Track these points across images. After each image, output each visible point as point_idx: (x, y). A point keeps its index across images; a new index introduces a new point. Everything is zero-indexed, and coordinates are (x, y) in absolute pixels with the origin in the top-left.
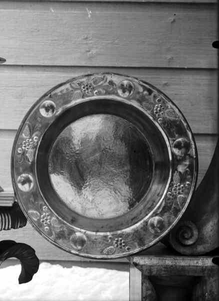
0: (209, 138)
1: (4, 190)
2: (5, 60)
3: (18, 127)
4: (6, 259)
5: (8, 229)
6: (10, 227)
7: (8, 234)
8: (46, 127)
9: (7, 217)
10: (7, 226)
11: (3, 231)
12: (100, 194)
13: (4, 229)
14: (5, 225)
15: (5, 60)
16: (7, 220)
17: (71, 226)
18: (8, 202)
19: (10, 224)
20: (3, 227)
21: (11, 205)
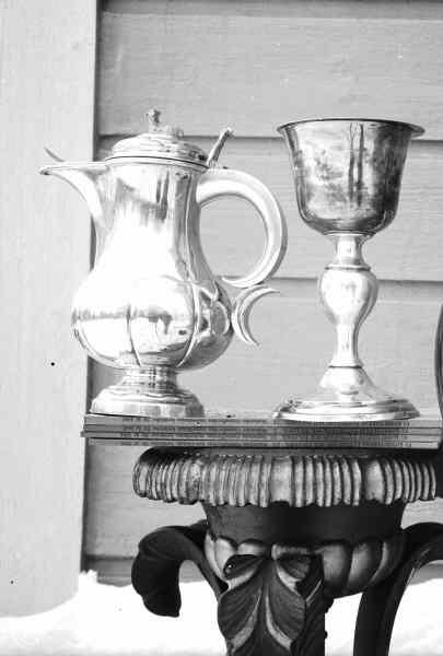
0: (218, 555)
1: (421, 413)
2: (421, 131)
3: (224, 412)
4: (424, 564)
5: (430, 498)
6: (433, 494)
7: (430, 509)
8: (348, 346)
9: (426, 472)
10: (413, 496)
11: (418, 502)
12: (420, 508)
13: (421, 499)
14: (416, 490)
15: (421, 131)
16: (427, 479)
17: (312, 594)
18: (430, 438)
19: (434, 487)
20: (419, 494)
21: (435, 446)
